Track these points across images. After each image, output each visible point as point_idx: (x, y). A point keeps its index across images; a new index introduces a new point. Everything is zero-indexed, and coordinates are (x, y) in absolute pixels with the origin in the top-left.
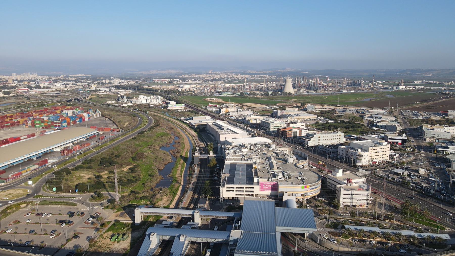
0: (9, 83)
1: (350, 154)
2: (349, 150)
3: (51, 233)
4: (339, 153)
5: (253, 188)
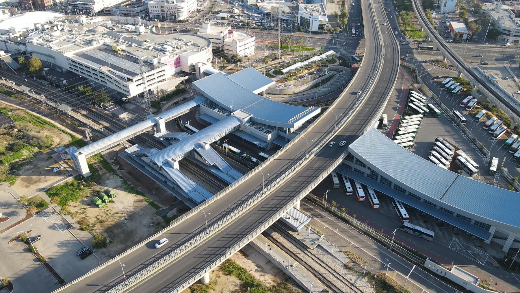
0: (244, 62)
1: (167, 9)
2: (166, 4)
3: (98, 206)
4: (150, 11)
5: (165, 74)
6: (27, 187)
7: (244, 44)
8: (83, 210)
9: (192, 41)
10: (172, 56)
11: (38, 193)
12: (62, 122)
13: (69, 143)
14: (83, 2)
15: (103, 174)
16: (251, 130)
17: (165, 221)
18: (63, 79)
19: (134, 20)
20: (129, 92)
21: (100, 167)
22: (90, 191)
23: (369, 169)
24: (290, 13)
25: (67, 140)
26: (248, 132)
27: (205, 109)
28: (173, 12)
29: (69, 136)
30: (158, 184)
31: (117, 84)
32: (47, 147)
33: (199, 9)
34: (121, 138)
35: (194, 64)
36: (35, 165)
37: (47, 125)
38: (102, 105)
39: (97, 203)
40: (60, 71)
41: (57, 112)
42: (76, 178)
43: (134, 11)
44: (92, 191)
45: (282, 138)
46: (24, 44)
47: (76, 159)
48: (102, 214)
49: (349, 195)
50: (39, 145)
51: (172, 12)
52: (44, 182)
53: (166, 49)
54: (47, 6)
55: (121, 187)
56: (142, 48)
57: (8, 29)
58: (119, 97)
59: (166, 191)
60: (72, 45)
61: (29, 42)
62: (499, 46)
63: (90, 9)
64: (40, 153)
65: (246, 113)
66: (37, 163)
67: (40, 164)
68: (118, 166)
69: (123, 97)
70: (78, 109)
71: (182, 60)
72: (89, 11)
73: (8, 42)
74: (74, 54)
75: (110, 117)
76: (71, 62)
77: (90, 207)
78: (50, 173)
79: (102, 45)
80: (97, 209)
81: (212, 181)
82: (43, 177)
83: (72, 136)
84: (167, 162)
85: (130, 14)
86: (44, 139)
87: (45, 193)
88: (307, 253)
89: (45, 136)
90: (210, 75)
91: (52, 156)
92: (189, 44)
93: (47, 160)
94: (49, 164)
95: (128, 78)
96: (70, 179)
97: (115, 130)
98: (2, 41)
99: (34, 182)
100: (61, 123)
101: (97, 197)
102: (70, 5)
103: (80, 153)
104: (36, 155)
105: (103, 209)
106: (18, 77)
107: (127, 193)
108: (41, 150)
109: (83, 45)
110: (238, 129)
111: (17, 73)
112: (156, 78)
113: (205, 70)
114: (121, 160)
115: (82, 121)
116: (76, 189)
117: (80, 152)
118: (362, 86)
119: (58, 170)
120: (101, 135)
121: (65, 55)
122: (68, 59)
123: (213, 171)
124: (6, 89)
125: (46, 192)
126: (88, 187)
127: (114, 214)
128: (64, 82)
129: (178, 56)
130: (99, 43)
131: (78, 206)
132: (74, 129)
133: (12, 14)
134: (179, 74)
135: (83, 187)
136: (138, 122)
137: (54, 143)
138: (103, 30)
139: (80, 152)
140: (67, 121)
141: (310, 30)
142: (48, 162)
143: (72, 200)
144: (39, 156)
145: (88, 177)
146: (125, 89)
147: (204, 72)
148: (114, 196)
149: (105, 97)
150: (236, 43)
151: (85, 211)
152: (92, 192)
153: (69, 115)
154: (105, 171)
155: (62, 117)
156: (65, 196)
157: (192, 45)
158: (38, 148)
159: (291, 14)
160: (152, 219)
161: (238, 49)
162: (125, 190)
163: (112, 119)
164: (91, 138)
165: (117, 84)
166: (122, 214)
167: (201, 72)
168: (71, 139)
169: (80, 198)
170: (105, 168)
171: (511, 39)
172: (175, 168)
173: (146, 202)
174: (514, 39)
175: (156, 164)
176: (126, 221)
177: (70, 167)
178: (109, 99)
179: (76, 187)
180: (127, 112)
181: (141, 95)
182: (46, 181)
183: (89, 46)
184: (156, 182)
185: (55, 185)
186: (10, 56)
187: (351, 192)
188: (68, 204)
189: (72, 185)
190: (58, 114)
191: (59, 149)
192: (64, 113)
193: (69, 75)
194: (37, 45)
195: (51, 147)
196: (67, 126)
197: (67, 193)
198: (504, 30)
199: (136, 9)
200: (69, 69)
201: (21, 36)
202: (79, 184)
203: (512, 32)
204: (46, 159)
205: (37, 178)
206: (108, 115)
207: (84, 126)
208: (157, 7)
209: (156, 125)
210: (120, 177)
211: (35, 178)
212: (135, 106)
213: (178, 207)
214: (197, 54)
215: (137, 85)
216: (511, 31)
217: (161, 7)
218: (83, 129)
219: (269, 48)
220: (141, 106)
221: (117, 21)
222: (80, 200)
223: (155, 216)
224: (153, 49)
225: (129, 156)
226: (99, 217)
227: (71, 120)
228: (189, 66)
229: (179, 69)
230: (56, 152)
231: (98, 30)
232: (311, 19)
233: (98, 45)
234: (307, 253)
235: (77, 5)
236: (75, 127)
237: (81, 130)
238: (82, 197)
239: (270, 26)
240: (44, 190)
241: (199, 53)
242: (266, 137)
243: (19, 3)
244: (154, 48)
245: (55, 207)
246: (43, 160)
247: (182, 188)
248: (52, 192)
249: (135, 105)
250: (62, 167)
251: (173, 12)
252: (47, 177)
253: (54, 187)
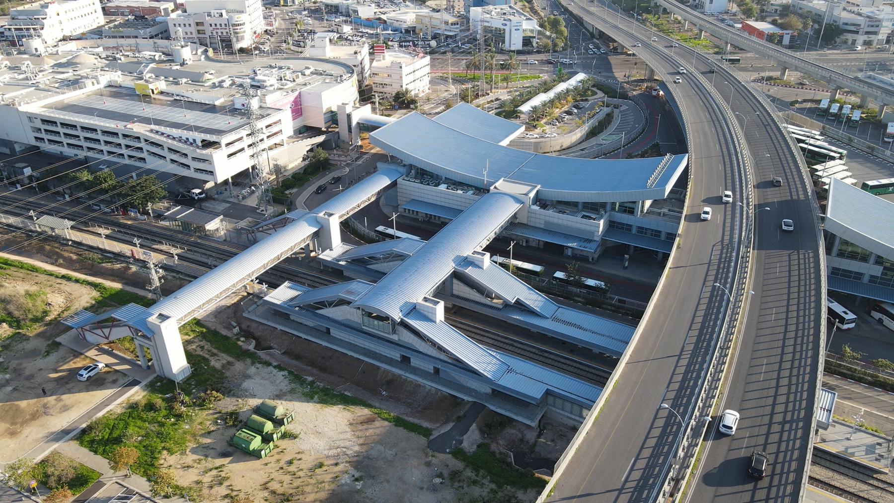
1: (211, 28)
6: (13, 434)
7: (412, 71)
8: (214, 472)
9: (311, 67)
10: (286, 93)
11: (55, 446)
12: (52, 257)
13: (94, 302)
14: (16, 25)
15: (223, 366)
16: (547, 219)
17: (467, 466)
18: (24, 165)
19: (155, 43)
20: (212, 173)
21: (209, 351)
22: (211, 417)
23: (879, 260)
24: (458, 24)
25: (85, 297)
26: (537, 225)
27: (413, 189)
28: (225, 34)
29: (88, 287)
30: (387, 372)
31: (175, 157)
32: (36, 320)
33: (270, 31)
34: (250, 272)
35: (334, 109)
36: (15, 370)
37: (12, 268)
39: (251, 448)
41: (29, 237)
42: (152, 387)
44: (216, 416)
45: (623, 228)
47: (151, 335)
48: (277, 476)
49: (849, 329)
50: (12, 317)
51: (222, 33)
52: (61, 413)
53: (264, 81)
55: (292, 391)
56: (206, 85)
58: (181, 190)
59: (418, 386)
62: (844, 51)
64: (18, 338)
65: (524, 184)
66: (20, 364)
67: (29, 367)
68: (254, 341)
69: (193, 189)
70: (86, 224)
71: (307, 102)
74: (43, 107)
75: (181, 232)
76: (38, 124)
77: (230, 463)
78: (69, 386)
80: (257, 463)
81: (515, 344)
82: (51, 400)
83: (95, 286)
84: (410, 307)
86: (22, 300)
87: (75, 444)
88: (875, 483)
89: (23, 293)
90: (378, 127)
91: (58, 340)
92: (307, 72)
93: (48, 353)
94: (58, 362)
95: (203, 141)
96: (137, 394)
97: (210, 261)
99: (28, 417)
100: (49, 260)
101: (244, 430)
103: (163, 317)
104: (9, 345)
105: (273, 459)
107: (318, 406)
108: (19, 328)
109: (57, 88)
110: (513, 223)
112: (246, 148)
113: (360, 119)
114: (254, 325)
115: (107, 248)
116: (167, 417)
117: (160, 315)
118: (708, 116)
119: (92, 374)
120: (174, 274)
121: (21, 109)
122: (31, 117)
123: (518, 317)
125: (77, 439)
126: (201, 404)
127: (312, 470)
128: (28, 171)
129: (296, 93)
130: (98, 83)
131: (195, 465)
132: (90, 270)
134: (300, 134)
135: (183, 409)
136: (259, 235)
137: (52, 309)
139: (160, 315)
140: (66, 254)
141: (506, 46)
142: (53, 358)
143: (168, 450)
144: (20, 346)
145: (187, 381)
146: (201, 166)
147: (358, 123)
148: (290, 420)
149: (153, 188)
150: (401, 67)
151: (223, 474)
152: (217, 419)
153: (68, 240)
154: (225, 358)
155: (48, 248)
156: (140, 442)
157: (312, 73)
158: (11, 326)
159: (458, 26)
160: (428, 464)
161: (406, 80)
162: (309, 397)
163: (186, 238)
164: (163, 281)
165: (175, 157)
166: (336, 464)
167: (354, 123)
168: (95, 294)
169: (189, 441)
170: (224, 352)
171: (861, 38)
172: (438, 321)
173: (384, 419)
174: (865, 37)
175: (384, 318)
176: (359, 485)
177: (123, 361)
178: (164, 193)
179: (164, 412)
180: (222, 217)
181: (243, 178)
182: (66, 408)
183: (75, 89)
184: (378, 368)
185: (100, 415)
187: (851, 321)
188: (162, 462)
189: (150, 407)
190: (34, 242)
191: (77, 319)
192: (51, 236)
193: (34, 155)
195: (48, 318)
196: (69, 264)
197: (143, 433)
198: (846, 24)
200: (33, 142)
202: (170, 401)
203: (862, 26)
204: (44, 350)
205: (35, 404)
206: (171, 230)
207: (118, 260)
208: (187, 25)
209: (321, 236)
210: (275, 367)
211: (29, 405)
212: (228, 205)
213: (478, 420)
214: (330, 90)
215: (230, 156)
216: (859, 25)
217: (198, 24)
218: (118, 266)
219: (457, 80)
220: (243, 203)
222: (192, 445)
223: (433, 456)
224: (231, 85)
225: (278, 313)
226: (274, 486)
227: (74, 250)
228: (325, 114)
229: (300, 123)
230: (69, 328)
232: (507, 28)
233: (97, 87)
234: (875, 483)
236: (93, 265)
237: (113, 270)
238: (194, 435)
239: (430, 47)
240: (72, 435)
241: (340, 85)
242: (592, 229)
244: (233, 84)
245: (123, 480)
246: (34, 354)
247: (475, 367)
248: (97, 435)
249: (228, 202)
250: (101, 365)
251: (225, 34)
252: (64, 397)
253: (98, 422)
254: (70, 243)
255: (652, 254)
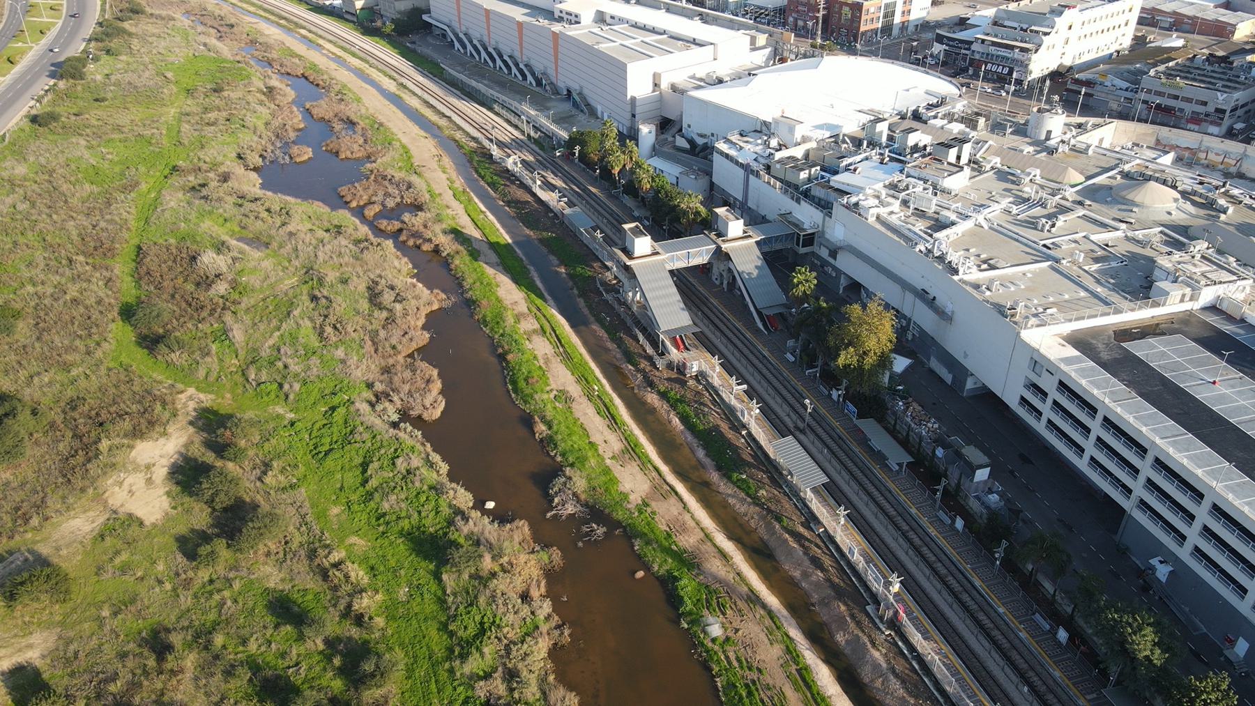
14: (996, 36)
38: (940, 487)
40: (948, 378)
43: (1205, 104)
46: (825, 207)
54: (864, 33)
57: (770, 120)
60: (1042, 270)
61: (847, 207)
63: (1012, 65)
72: (1006, 71)
73: (757, 175)
76: (1048, 384)
79: (1205, 309)
85: (1181, 110)
98: (737, 163)
102: (940, 39)
106: (766, 353)
111: (760, 325)
115: (838, 539)
124: (715, 418)
133: (779, 57)
138: (1171, 206)
186: (758, 243)
194: (878, 226)
199: (1221, 97)
201: (808, 160)
221: (1187, 154)
231: (1147, 202)
233: (1187, 306)
235: (970, 43)
243: (781, 12)
254: (744, 433)
255: (1142, 24)
